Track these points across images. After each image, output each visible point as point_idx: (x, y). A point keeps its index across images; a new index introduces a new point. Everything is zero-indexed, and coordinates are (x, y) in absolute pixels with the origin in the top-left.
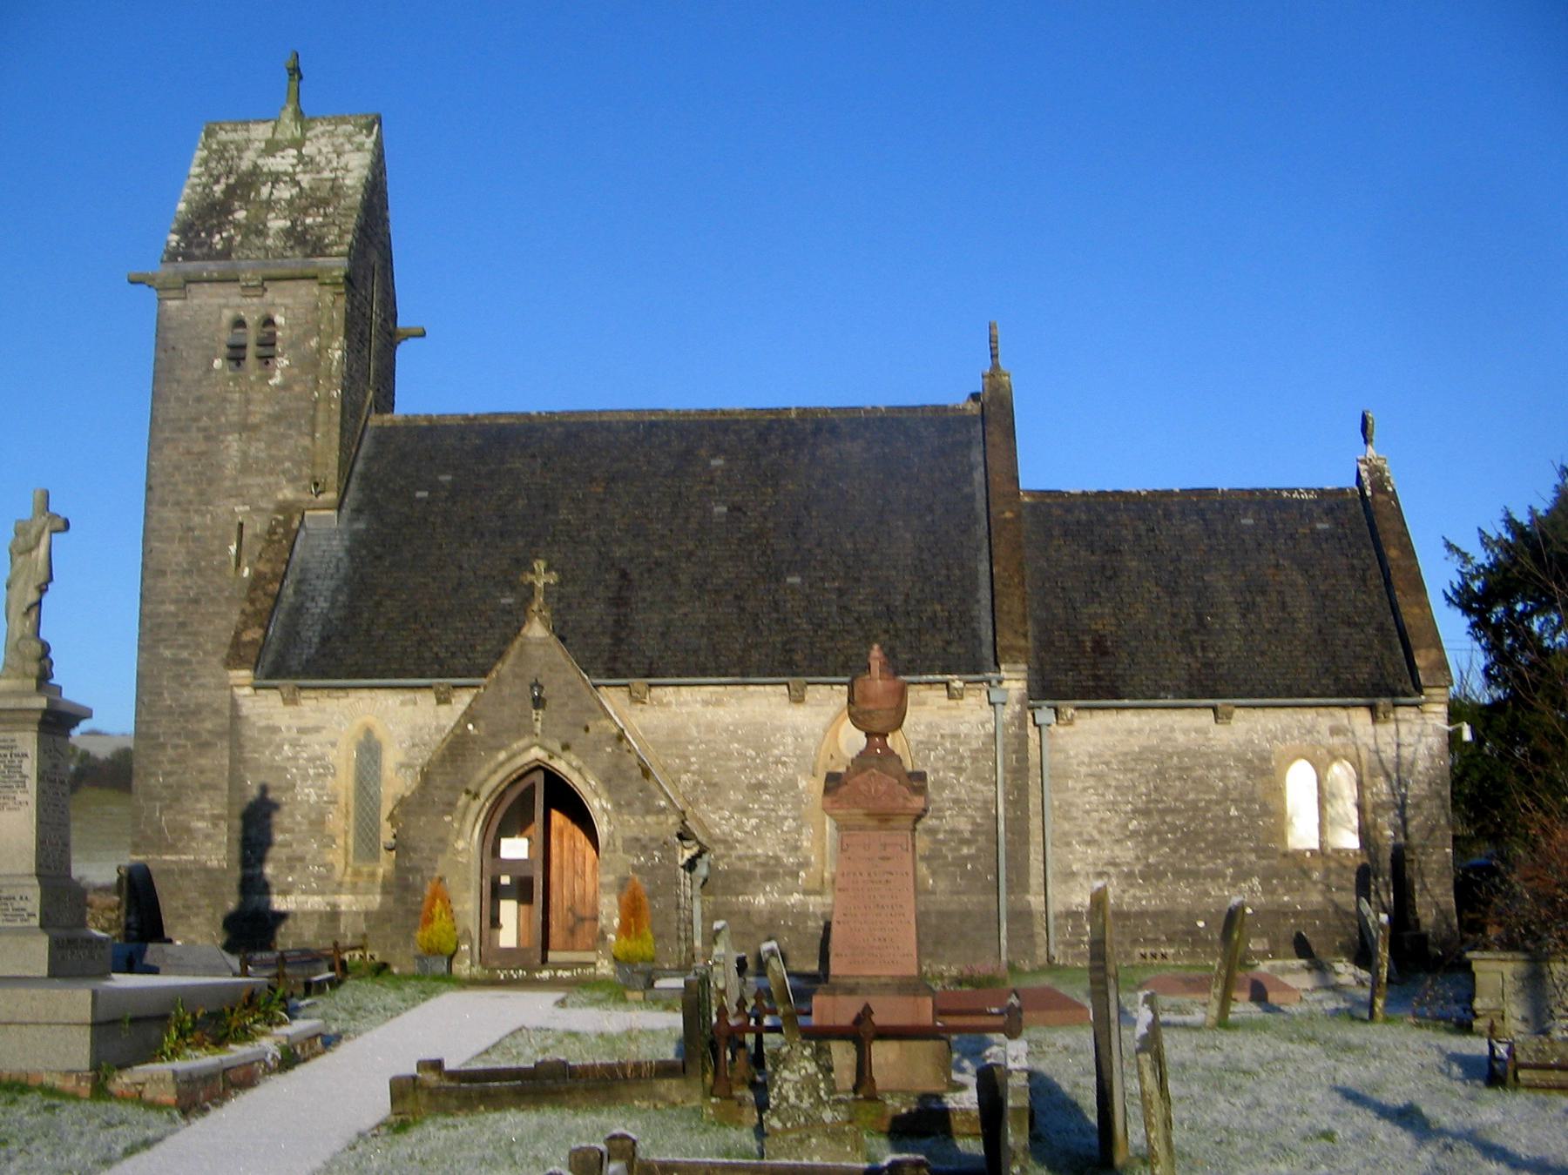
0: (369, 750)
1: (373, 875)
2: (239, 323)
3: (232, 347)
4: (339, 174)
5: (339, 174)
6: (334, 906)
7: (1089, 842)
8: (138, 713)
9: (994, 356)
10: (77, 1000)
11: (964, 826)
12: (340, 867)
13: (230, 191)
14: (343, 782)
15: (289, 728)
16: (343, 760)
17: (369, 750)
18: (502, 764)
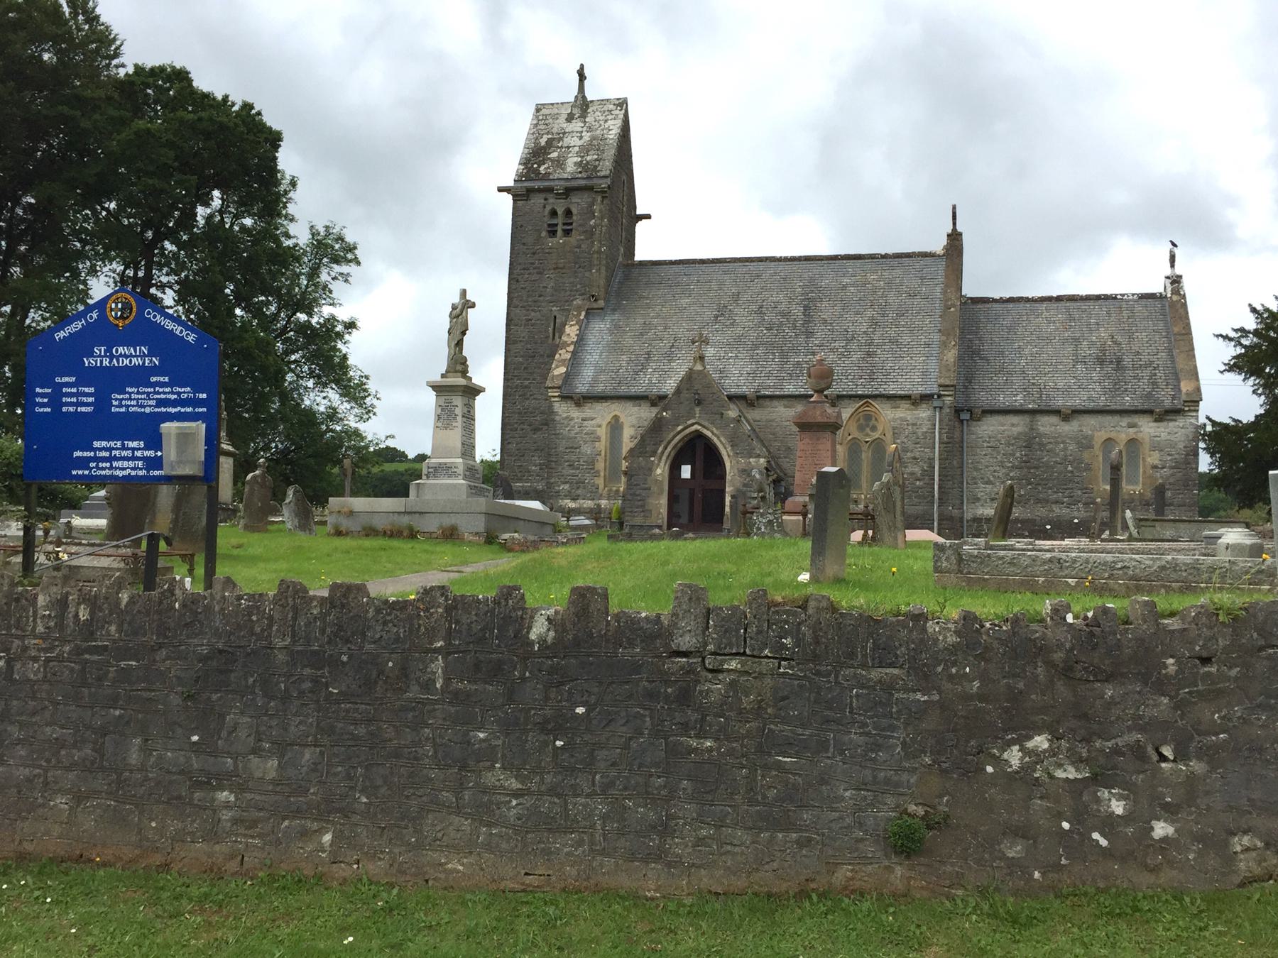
1: (617, 491)
2: (554, 213)
3: (549, 225)
6: (599, 506)
7: (989, 482)
9: (954, 224)
10: (481, 503)
11: (917, 470)
12: (601, 486)
13: (550, 142)
14: (602, 446)
16: (602, 432)
18: (679, 432)
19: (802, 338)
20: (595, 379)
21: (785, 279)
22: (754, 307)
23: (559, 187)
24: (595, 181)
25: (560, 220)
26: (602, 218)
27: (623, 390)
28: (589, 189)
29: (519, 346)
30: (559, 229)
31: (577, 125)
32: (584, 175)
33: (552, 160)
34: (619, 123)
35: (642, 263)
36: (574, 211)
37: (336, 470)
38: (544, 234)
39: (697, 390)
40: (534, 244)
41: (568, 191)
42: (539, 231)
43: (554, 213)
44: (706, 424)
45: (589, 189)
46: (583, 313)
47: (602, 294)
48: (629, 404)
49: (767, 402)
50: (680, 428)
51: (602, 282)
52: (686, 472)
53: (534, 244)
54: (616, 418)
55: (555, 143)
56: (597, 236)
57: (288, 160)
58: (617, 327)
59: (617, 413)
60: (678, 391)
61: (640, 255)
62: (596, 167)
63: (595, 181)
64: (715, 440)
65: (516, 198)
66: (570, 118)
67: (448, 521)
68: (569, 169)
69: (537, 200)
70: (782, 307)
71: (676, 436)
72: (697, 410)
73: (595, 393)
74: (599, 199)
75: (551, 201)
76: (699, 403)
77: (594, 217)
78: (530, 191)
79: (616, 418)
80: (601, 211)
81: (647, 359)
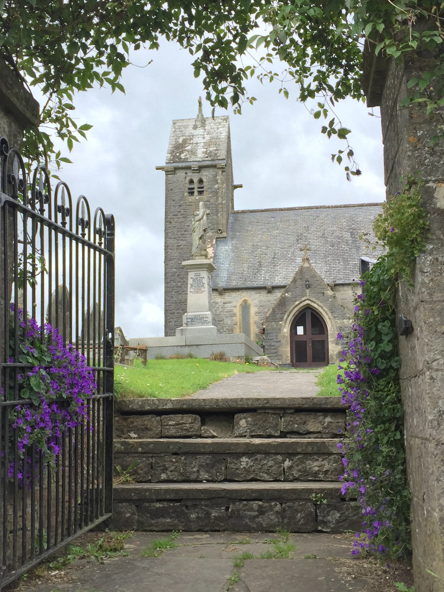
0: (245, 307)
2: (191, 182)
3: (189, 189)
4: (219, 134)
5: (219, 134)
8: (165, 303)
14: (238, 318)
15: (221, 302)
16: (238, 311)
17: (245, 307)
18: (297, 306)
19: (354, 250)
20: (229, 278)
21: (335, 218)
22: (320, 234)
23: (195, 166)
24: (217, 162)
25: (196, 185)
26: (222, 184)
27: (249, 284)
28: (215, 166)
29: (173, 262)
30: (196, 191)
31: (200, 131)
32: (209, 159)
33: (188, 151)
34: (226, 129)
35: (238, 212)
36: (204, 180)
37: (396, 231)
38: (186, 194)
39: (305, 279)
40: (180, 200)
41: (201, 168)
42: (183, 193)
43: (191, 182)
44: (314, 299)
45: (215, 166)
46: (214, 240)
47: (225, 228)
48: (253, 293)
49: (341, 288)
50: (297, 303)
51: (224, 222)
52: (300, 330)
53: (180, 200)
54: (245, 301)
55: (188, 141)
56: (220, 194)
57: (88, 124)
58: (236, 248)
59: (245, 298)
60: (294, 281)
61: (237, 208)
62: (216, 154)
63: (217, 162)
64: (320, 309)
65: (168, 172)
66: (195, 127)
67: (217, 350)
68: (199, 156)
69: (181, 174)
70: (337, 233)
71: (294, 309)
72: (308, 291)
73: (231, 287)
74: (220, 172)
75: (190, 174)
76: (308, 287)
77: (217, 183)
78: (176, 169)
79: (245, 301)
80: (221, 179)
81: (260, 265)
